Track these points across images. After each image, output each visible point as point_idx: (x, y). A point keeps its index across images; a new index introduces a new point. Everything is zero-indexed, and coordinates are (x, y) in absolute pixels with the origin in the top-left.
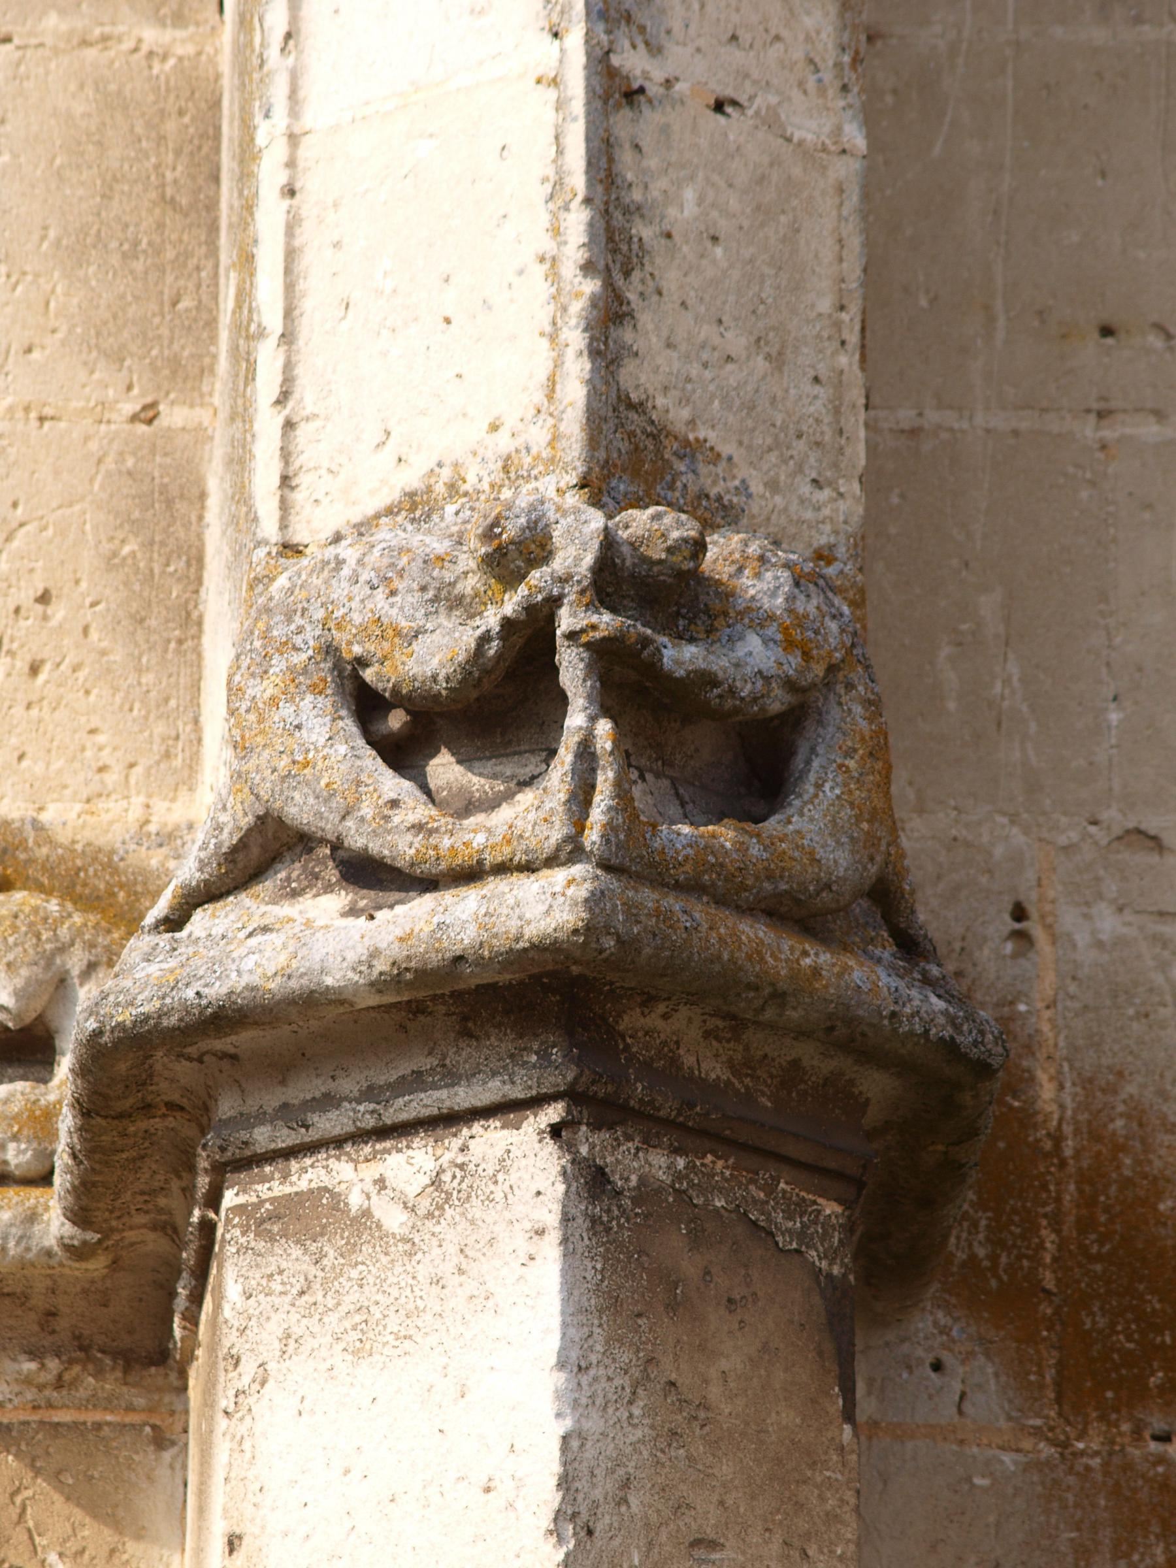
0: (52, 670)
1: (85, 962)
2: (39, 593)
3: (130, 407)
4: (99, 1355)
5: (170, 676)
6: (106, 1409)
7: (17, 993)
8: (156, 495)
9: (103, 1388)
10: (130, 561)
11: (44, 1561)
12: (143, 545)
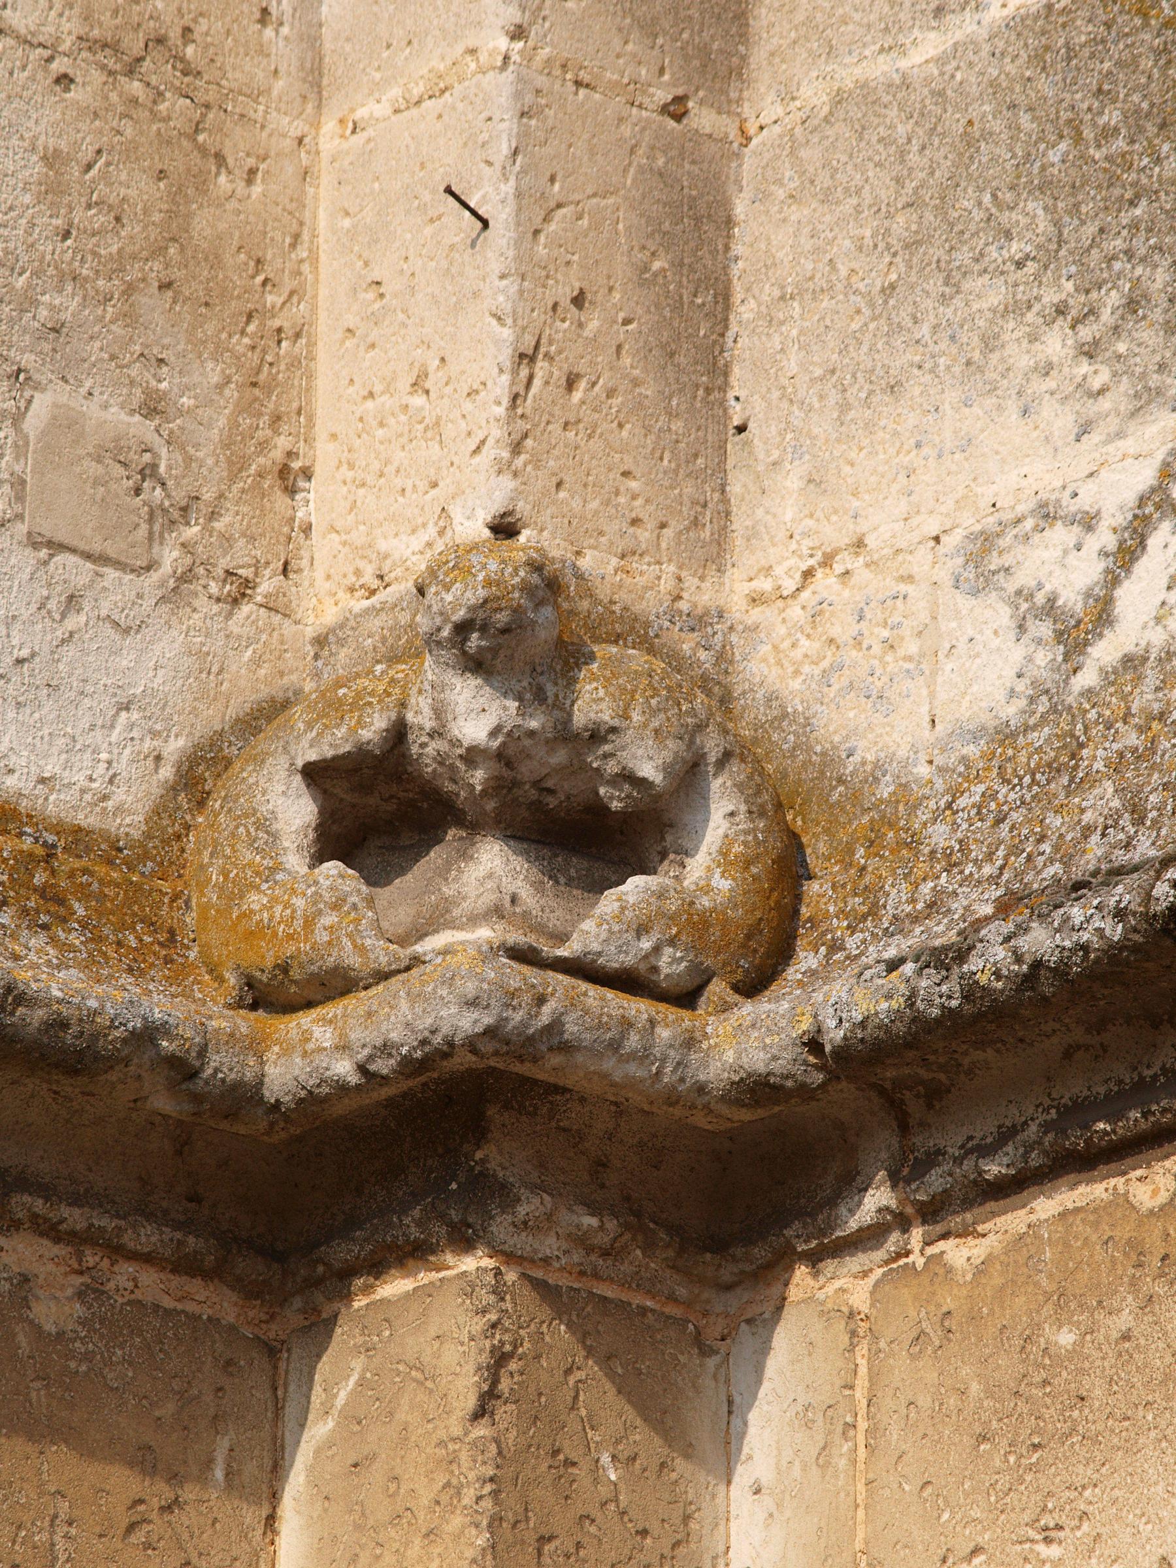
0: (587, 390)
1: (721, 749)
2: (575, 293)
3: (663, 96)
4: (652, 1225)
5: (699, 429)
6: (649, 1292)
7: (666, 769)
8: (686, 208)
9: (647, 1267)
10: (660, 280)
11: (598, 1461)
12: (672, 264)
